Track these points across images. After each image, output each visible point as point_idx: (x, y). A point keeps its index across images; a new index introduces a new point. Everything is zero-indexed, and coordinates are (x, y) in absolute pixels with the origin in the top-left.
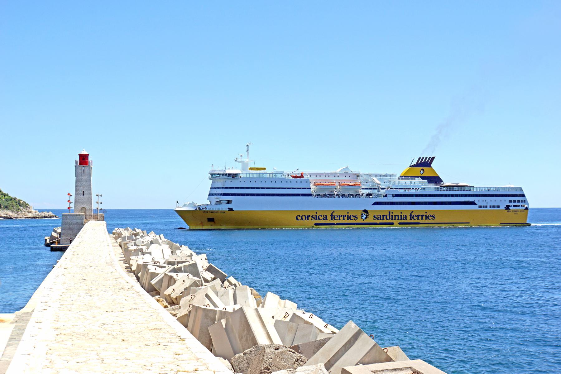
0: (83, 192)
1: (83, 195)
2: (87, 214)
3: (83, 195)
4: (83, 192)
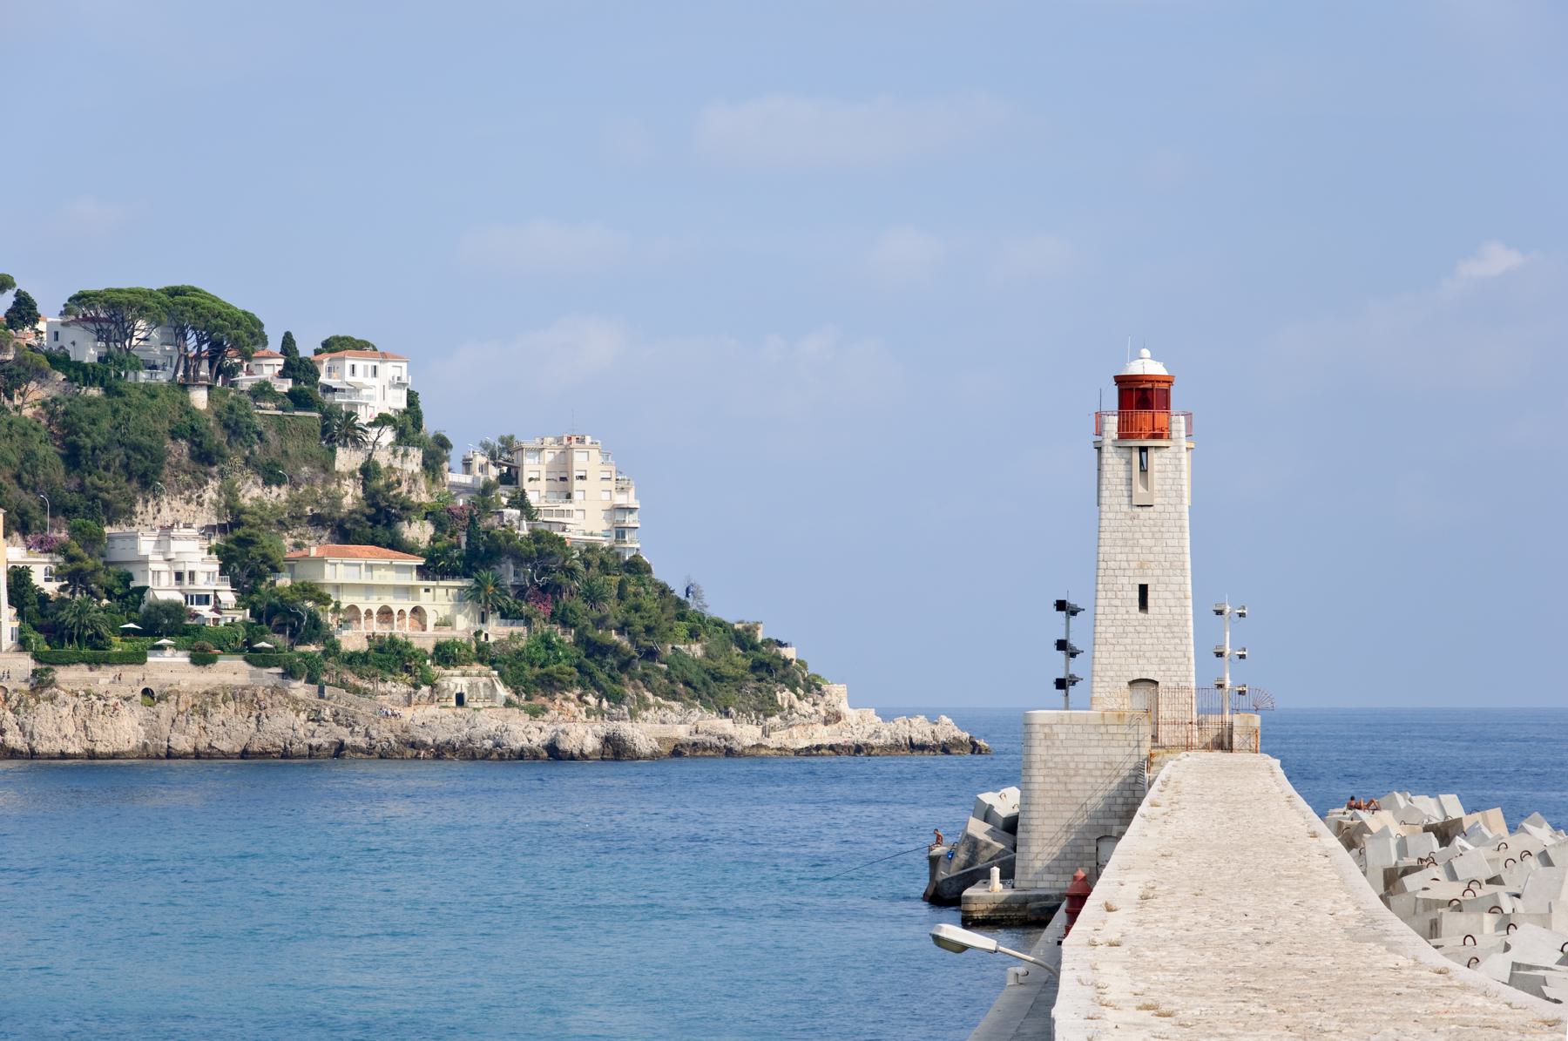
0: (1143, 590)
1: (1143, 604)
2: (1165, 713)
3: (1143, 604)
4: (1143, 590)
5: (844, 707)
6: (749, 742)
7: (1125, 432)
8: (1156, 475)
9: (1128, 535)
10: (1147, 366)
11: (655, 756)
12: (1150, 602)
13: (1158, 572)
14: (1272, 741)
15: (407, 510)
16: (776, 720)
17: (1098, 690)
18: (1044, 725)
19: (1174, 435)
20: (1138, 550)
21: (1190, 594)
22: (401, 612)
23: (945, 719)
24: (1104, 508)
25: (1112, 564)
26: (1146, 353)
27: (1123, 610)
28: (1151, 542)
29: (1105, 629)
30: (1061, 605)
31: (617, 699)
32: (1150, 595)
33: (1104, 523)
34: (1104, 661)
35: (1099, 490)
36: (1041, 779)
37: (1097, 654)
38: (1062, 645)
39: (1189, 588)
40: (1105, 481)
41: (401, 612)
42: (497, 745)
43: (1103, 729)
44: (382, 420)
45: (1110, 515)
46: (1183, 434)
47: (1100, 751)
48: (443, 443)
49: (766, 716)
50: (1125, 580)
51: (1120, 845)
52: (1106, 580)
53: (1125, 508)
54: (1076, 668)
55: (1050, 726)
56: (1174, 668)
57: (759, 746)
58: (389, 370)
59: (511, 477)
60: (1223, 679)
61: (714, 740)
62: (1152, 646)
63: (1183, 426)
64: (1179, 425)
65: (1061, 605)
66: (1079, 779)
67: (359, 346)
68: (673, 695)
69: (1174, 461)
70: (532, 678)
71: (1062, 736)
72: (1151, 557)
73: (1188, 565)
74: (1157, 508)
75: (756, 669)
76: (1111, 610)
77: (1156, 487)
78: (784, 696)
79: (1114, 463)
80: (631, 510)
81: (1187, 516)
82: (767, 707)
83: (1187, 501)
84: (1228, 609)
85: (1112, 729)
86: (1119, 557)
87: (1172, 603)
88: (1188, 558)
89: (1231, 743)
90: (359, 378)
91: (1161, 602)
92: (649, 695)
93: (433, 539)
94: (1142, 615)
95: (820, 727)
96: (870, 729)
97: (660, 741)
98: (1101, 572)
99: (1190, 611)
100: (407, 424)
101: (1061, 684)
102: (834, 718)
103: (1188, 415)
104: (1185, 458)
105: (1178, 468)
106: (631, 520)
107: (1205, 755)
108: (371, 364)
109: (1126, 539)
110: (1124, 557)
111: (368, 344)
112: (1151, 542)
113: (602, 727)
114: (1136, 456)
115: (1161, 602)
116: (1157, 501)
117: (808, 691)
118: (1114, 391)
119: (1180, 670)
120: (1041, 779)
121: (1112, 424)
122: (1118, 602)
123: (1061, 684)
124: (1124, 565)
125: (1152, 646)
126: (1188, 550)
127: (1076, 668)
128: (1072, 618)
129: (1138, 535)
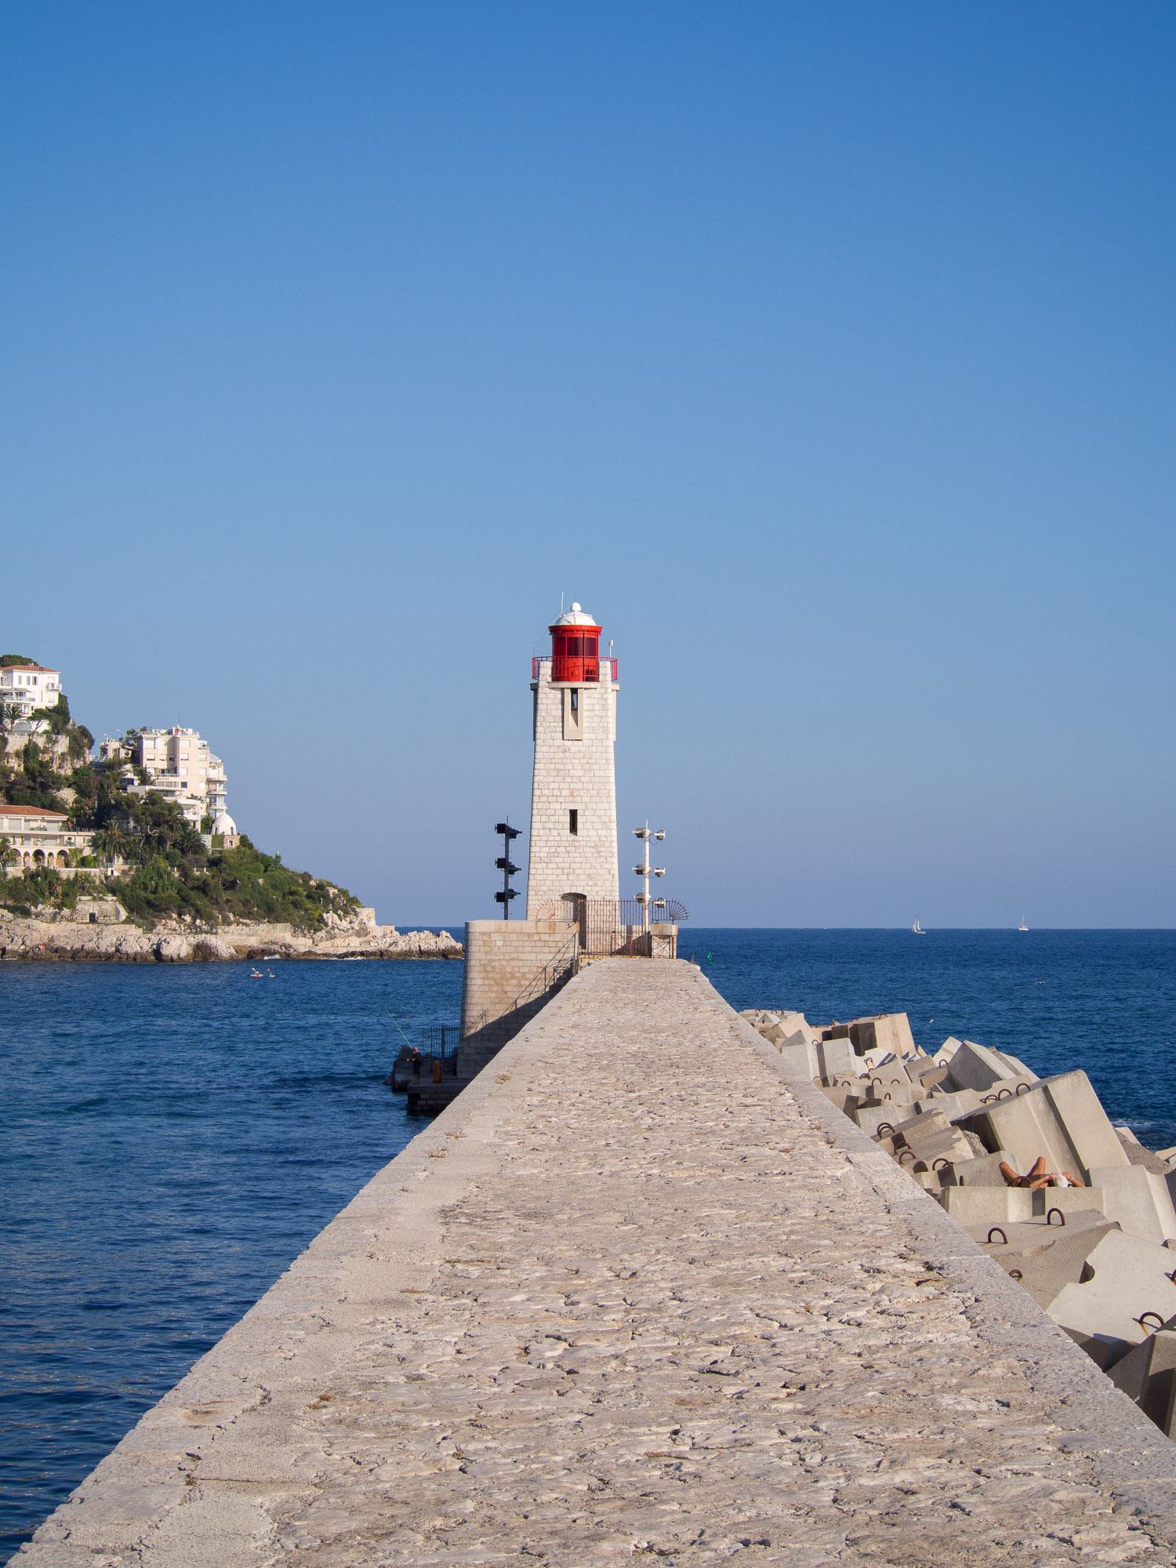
0: (573, 814)
1: (573, 828)
3: (573, 828)
4: (573, 814)
5: (372, 924)
6: (302, 950)
7: (558, 675)
8: (585, 714)
9: (561, 767)
10: (579, 618)
11: (232, 961)
12: (579, 826)
13: (587, 799)
14: (692, 947)
15: (59, 782)
16: (322, 934)
17: (534, 903)
18: (484, 934)
19: (601, 678)
20: (569, 780)
21: (614, 818)
22: (51, 854)
23: (444, 933)
24: (538, 742)
25: (545, 792)
26: (577, 607)
27: (554, 832)
28: (581, 773)
29: (539, 850)
30: (501, 828)
31: (209, 918)
32: (580, 819)
33: (538, 755)
34: (538, 877)
35: (535, 726)
36: (480, 982)
37: (532, 871)
38: (502, 863)
39: (614, 813)
40: (539, 718)
41: (51, 854)
42: (117, 950)
43: (536, 938)
44: (39, 715)
45: (544, 749)
46: (609, 678)
47: (533, 956)
48: (84, 732)
49: (316, 931)
50: (558, 806)
51: (204, 1365)
52: (540, 806)
53: (559, 742)
54: (514, 882)
55: (489, 934)
56: (600, 883)
57: (310, 952)
58: (45, 678)
59: (136, 758)
60: (643, 894)
61: (277, 948)
62: (580, 856)
63: (609, 671)
64: (605, 669)
65: (501, 828)
66: (514, 982)
67: (24, 662)
68: (249, 915)
69: (600, 699)
70: (144, 905)
71: (499, 943)
72: (580, 786)
73: (613, 793)
74: (586, 742)
75: (305, 900)
76: (545, 833)
77: (585, 724)
78: (330, 917)
79: (550, 698)
80: (220, 782)
81: (612, 750)
82: (315, 924)
83: (612, 737)
84: (648, 832)
85: (545, 937)
86: (552, 786)
87: (599, 826)
88: (613, 787)
89: (650, 950)
90: (24, 686)
91: (589, 826)
92: (231, 915)
93: (76, 801)
94: (572, 837)
95: (354, 938)
96: (389, 940)
97: (238, 949)
98: (536, 799)
99: (615, 833)
100: (58, 716)
101: (502, 897)
102: (363, 932)
103: (614, 662)
104: (612, 699)
105: (605, 708)
106: (220, 789)
107: (619, 961)
108: (32, 675)
109: (559, 770)
110: (556, 786)
111: (30, 661)
112: (581, 773)
113: (194, 940)
114: (568, 693)
115: (589, 826)
116: (585, 736)
117: (346, 913)
118: (549, 640)
119: (603, 886)
120: (480, 982)
121: (547, 668)
122: (551, 826)
123: (502, 897)
124: (557, 792)
125: (580, 856)
126: (613, 780)
127: (514, 882)
128: (511, 841)
129: (569, 766)
